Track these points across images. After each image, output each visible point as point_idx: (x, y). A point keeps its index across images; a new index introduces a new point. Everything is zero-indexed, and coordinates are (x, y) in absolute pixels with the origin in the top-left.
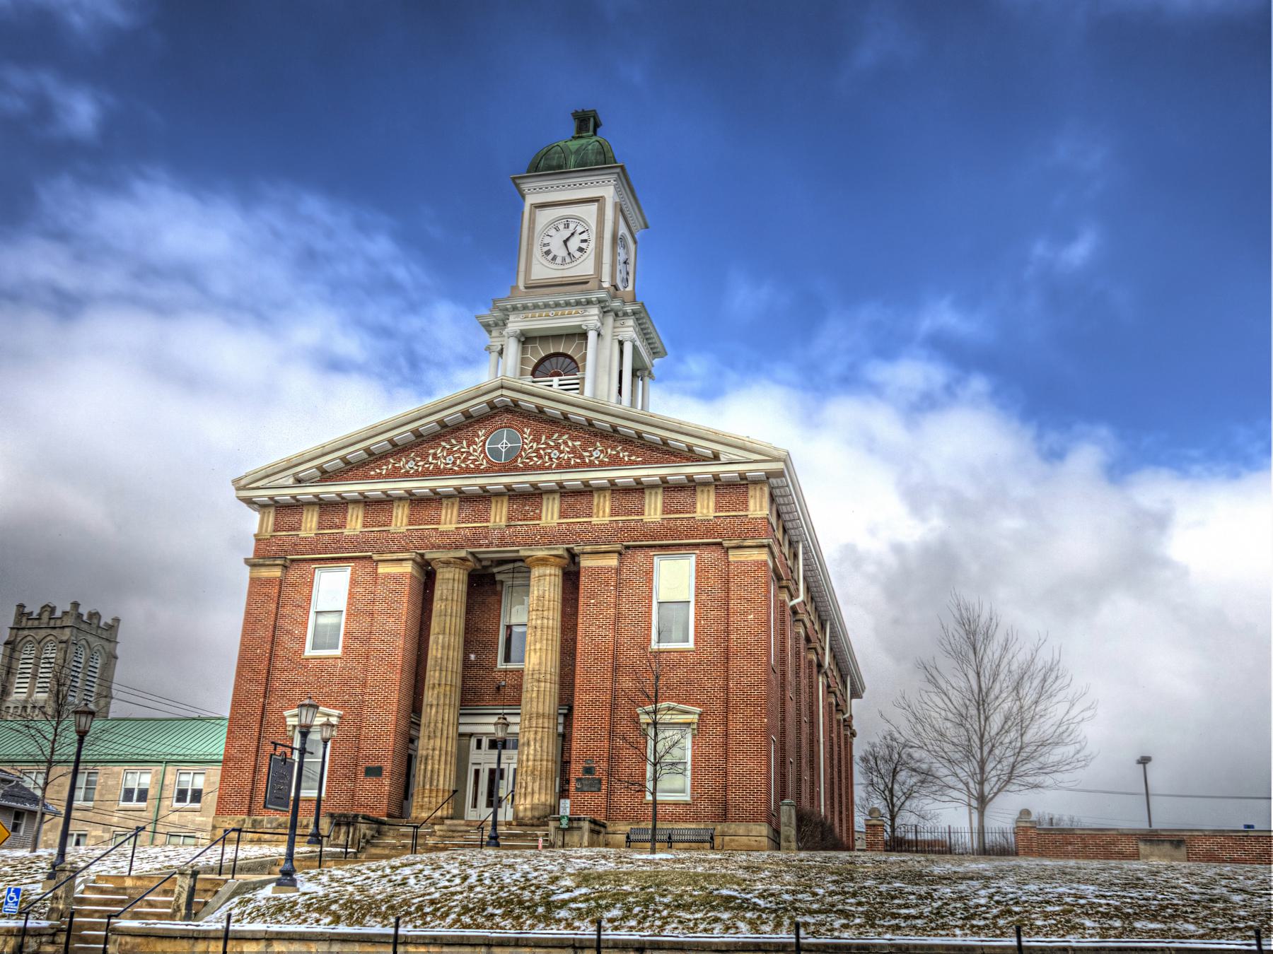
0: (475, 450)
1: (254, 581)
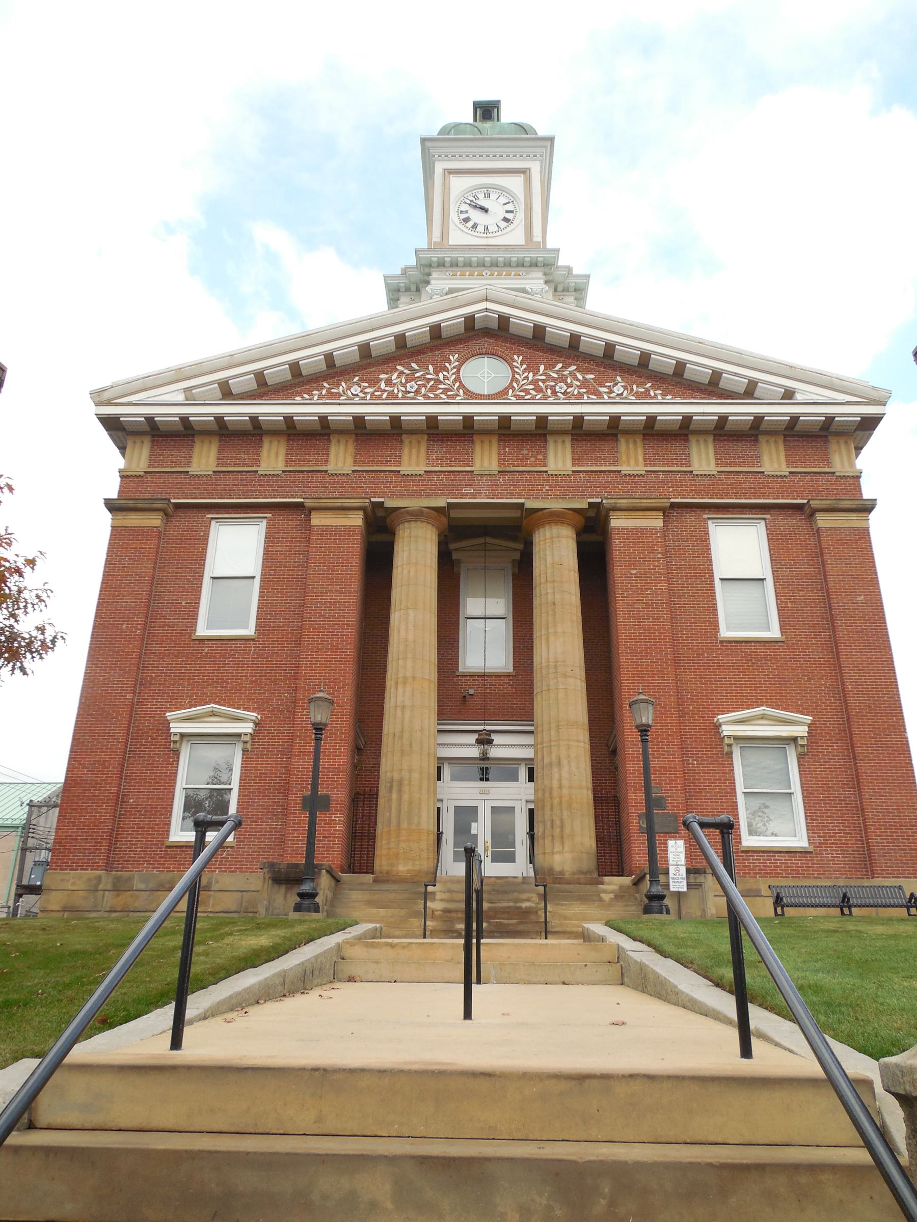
0: (445, 377)
1: (117, 533)
